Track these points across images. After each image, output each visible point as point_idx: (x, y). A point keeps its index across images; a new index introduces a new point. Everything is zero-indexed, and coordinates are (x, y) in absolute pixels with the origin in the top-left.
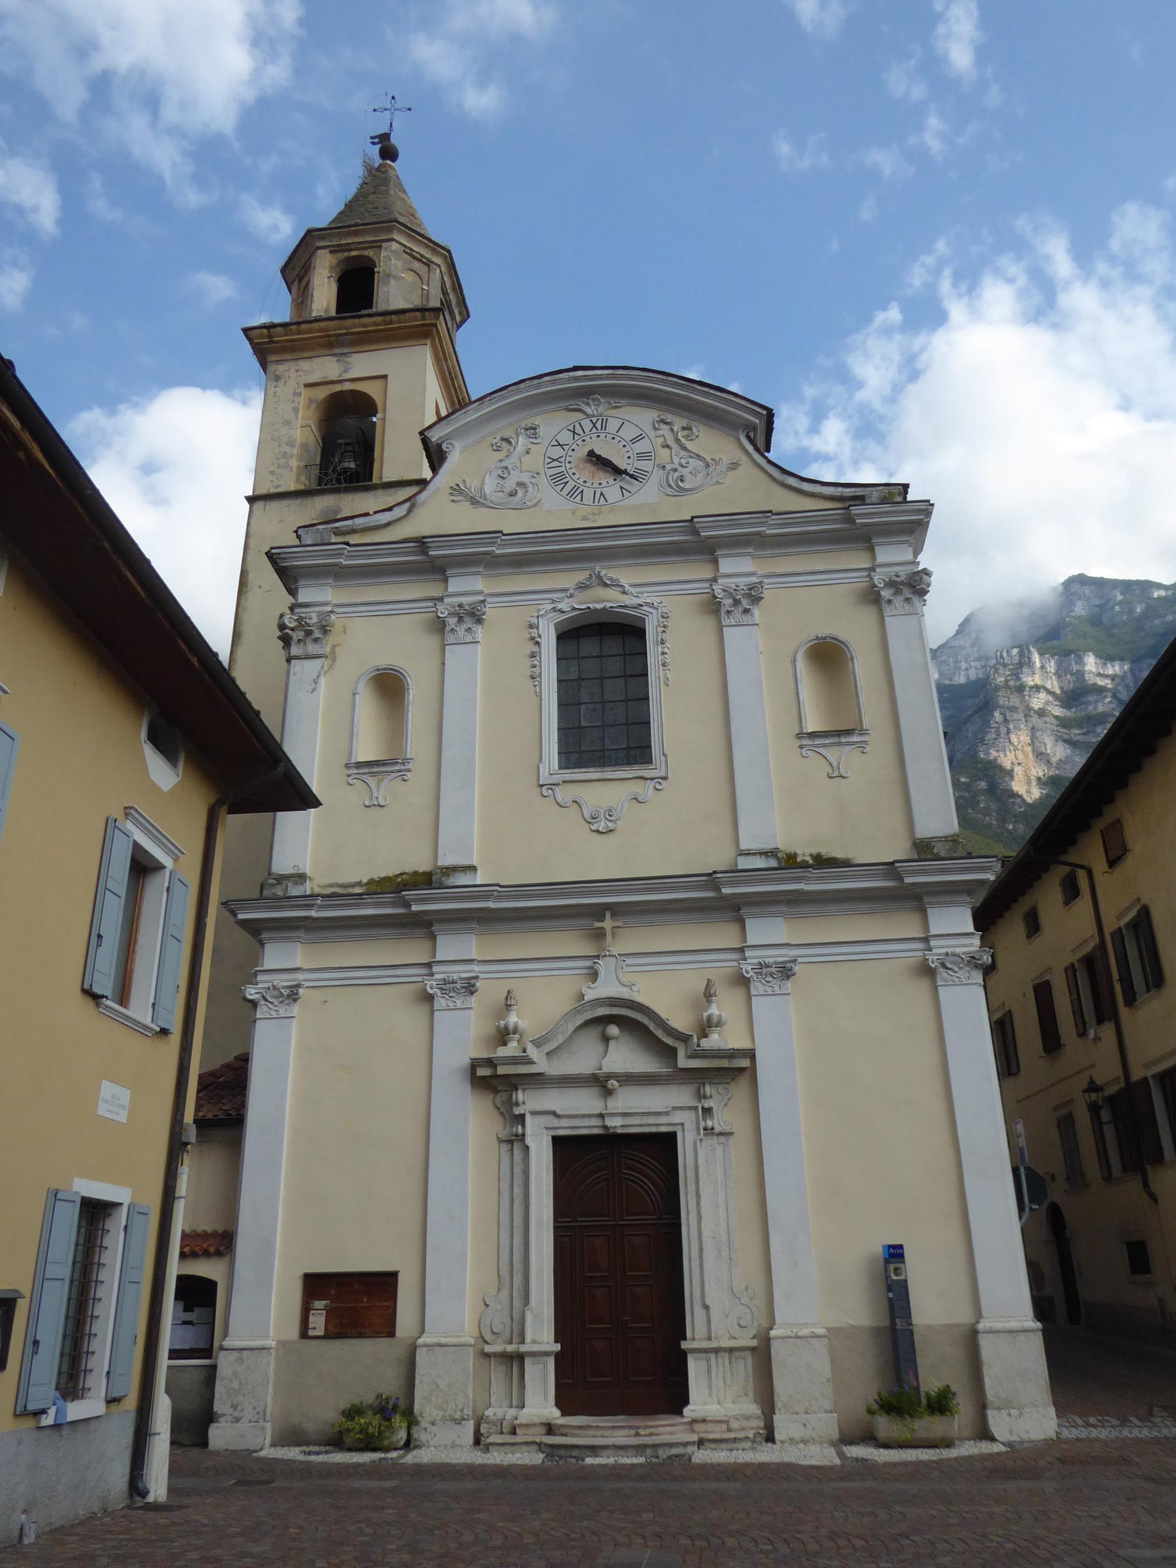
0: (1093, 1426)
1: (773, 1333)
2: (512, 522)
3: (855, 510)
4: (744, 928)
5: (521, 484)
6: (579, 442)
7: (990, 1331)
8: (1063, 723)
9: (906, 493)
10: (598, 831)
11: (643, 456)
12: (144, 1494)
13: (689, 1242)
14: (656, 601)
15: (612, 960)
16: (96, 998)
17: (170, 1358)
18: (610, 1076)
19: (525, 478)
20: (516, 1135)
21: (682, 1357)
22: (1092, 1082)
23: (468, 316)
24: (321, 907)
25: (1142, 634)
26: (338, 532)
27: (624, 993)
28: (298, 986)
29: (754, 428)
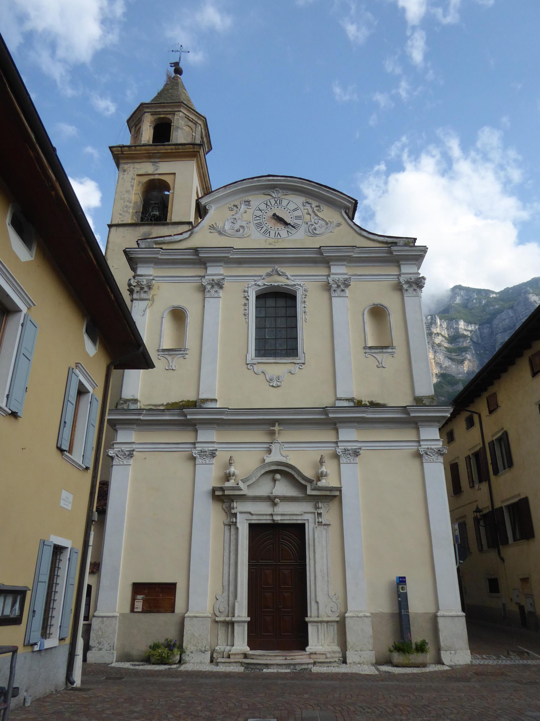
0: (485, 659)
1: (347, 615)
2: (238, 244)
3: (393, 248)
4: (338, 433)
5: (242, 227)
6: (269, 209)
7: (443, 616)
8: (448, 350)
9: (415, 242)
10: (273, 386)
11: (298, 218)
12: (72, 683)
13: (310, 572)
14: (302, 283)
15: (278, 445)
16: (61, 451)
17: (84, 620)
18: (276, 497)
19: (244, 224)
20: (233, 522)
21: (305, 626)
22: (477, 508)
23: (212, 149)
24: (145, 415)
25: (484, 313)
26: (157, 243)
27: (283, 460)
28: (133, 450)
29: (349, 209)
